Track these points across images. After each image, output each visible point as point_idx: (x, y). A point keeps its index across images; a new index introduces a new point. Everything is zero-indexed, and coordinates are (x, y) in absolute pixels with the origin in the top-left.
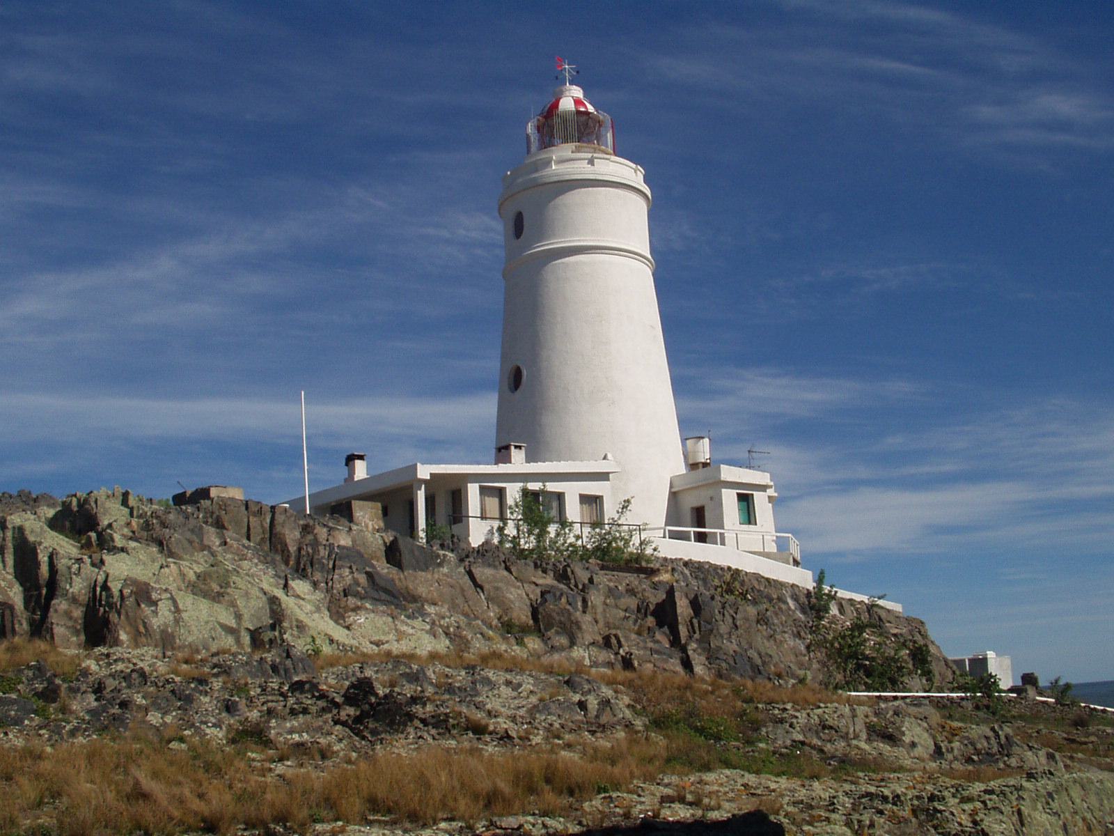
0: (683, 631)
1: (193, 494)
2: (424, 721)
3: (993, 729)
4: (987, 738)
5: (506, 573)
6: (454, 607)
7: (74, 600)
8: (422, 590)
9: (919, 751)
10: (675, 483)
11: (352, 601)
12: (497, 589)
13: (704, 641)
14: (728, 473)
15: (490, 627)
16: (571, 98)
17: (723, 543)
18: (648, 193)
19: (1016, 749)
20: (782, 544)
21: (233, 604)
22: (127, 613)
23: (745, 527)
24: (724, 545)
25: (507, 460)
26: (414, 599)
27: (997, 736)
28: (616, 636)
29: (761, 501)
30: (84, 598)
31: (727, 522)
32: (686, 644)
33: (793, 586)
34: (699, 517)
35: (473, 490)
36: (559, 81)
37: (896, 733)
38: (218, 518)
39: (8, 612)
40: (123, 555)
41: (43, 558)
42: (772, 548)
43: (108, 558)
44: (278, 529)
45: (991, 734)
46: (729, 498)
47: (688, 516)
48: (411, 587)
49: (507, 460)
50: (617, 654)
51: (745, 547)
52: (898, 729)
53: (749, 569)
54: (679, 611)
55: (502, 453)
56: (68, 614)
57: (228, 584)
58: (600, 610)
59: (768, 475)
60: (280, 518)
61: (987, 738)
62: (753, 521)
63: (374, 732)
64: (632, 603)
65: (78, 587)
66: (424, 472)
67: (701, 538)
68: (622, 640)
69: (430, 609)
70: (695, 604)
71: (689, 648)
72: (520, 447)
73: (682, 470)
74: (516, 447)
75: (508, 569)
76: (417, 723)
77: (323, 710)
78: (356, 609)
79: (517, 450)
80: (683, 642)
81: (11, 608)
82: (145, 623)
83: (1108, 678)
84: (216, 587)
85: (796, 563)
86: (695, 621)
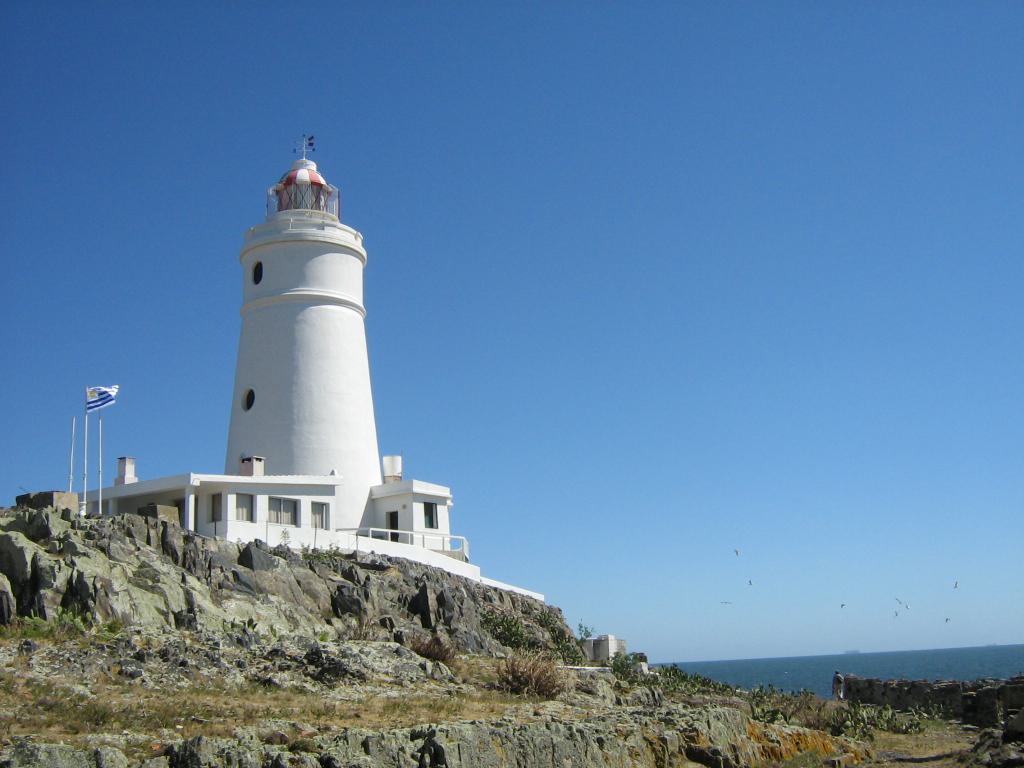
0: (432, 616)
1: (36, 496)
2: (352, 674)
3: (650, 689)
4: (647, 695)
5: (311, 572)
6: (285, 597)
7: (57, 591)
8: (266, 584)
9: (608, 701)
10: (375, 492)
11: (225, 592)
12: (309, 583)
13: (447, 622)
14: (421, 487)
15: (311, 612)
16: (308, 172)
17: (412, 543)
18: (364, 253)
19: (664, 703)
20: (455, 543)
21: (162, 594)
22: (100, 601)
23: (429, 530)
24: (327, 528)
25: (250, 473)
26: (261, 591)
27: (653, 695)
28: (390, 620)
29: (442, 513)
30: (64, 589)
31: (415, 528)
32: (435, 626)
33: (466, 579)
34: (393, 520)
35: (231, 500)
36: (296, 154)
37: (595, 690)
38: (129, 529)
39: (4, 597)
40: (85, 558)
41: (29, 559)
42: (448, 547)
43: (76, 559)
44: (169, 539)
45: (648, 692)
46: (418, 509)
47: (384, 518)
48: (259, 582)
49: (250, 473)
50: (391, 632)
51: (427, 548)
52: (594, 687)
53: (435, 564)
54: (430, 602)
55: (245, 464)
56: (53, 600)
57: (158, 581)
58: (376, 600)
59: (448, 489)
60: (170, 531)
61: (647, 695)
62: (435, 524)
63: (329, 681)
64: (394, 595)
65: (60, 581)
66: (196, 479)
67: (395, 538)
68: (394, 622)
69: (272, 598)
70: (441, 599)
71: (438, 629)
72: (260, 460)
73: (379, 482)
74: (257, 459)
75: (312, 568)
76: (349, 676)
77: (297, 667)
78: (229, 598)
79: (258, 462)
80: (433, 624)
81: (7, 594)
82: (112, 608)
83: (1019, 641)
84: (150, 583)
85: (467, 560)
86: (441, 610)
